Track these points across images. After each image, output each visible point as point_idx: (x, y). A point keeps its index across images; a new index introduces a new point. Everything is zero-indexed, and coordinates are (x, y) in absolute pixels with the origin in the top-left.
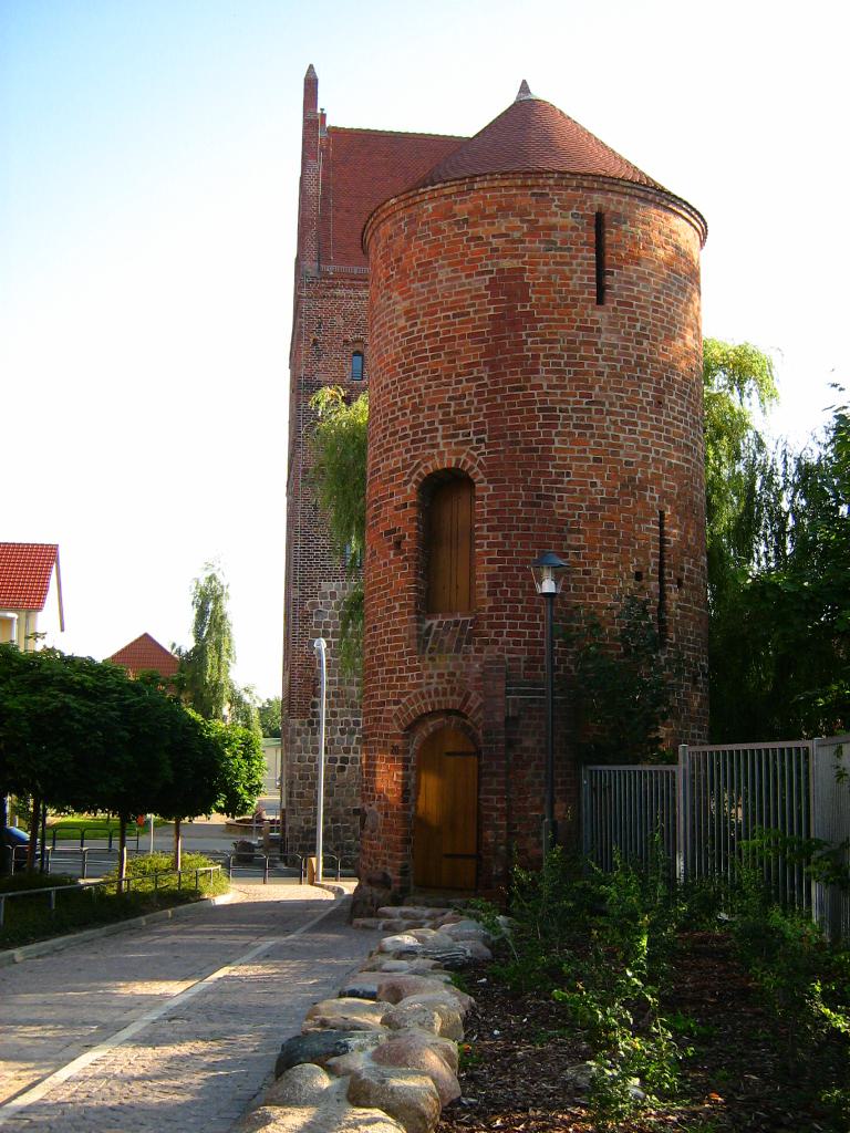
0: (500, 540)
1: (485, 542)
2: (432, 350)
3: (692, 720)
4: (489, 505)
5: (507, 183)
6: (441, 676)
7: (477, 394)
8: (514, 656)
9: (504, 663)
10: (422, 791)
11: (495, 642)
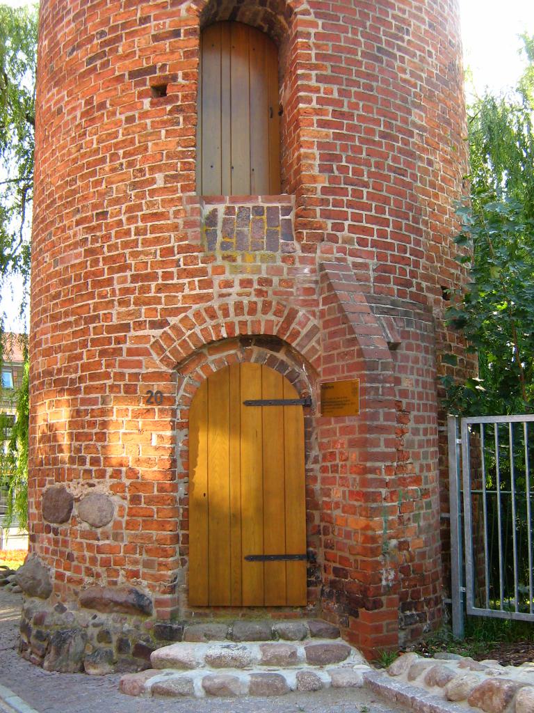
0: (336, 95)
1: (314, 96)
4: (317, 47)
6: (246, 283)
8: (360, 260)
9: (346, 268)
10: (201, 460)
11: (333, 239)
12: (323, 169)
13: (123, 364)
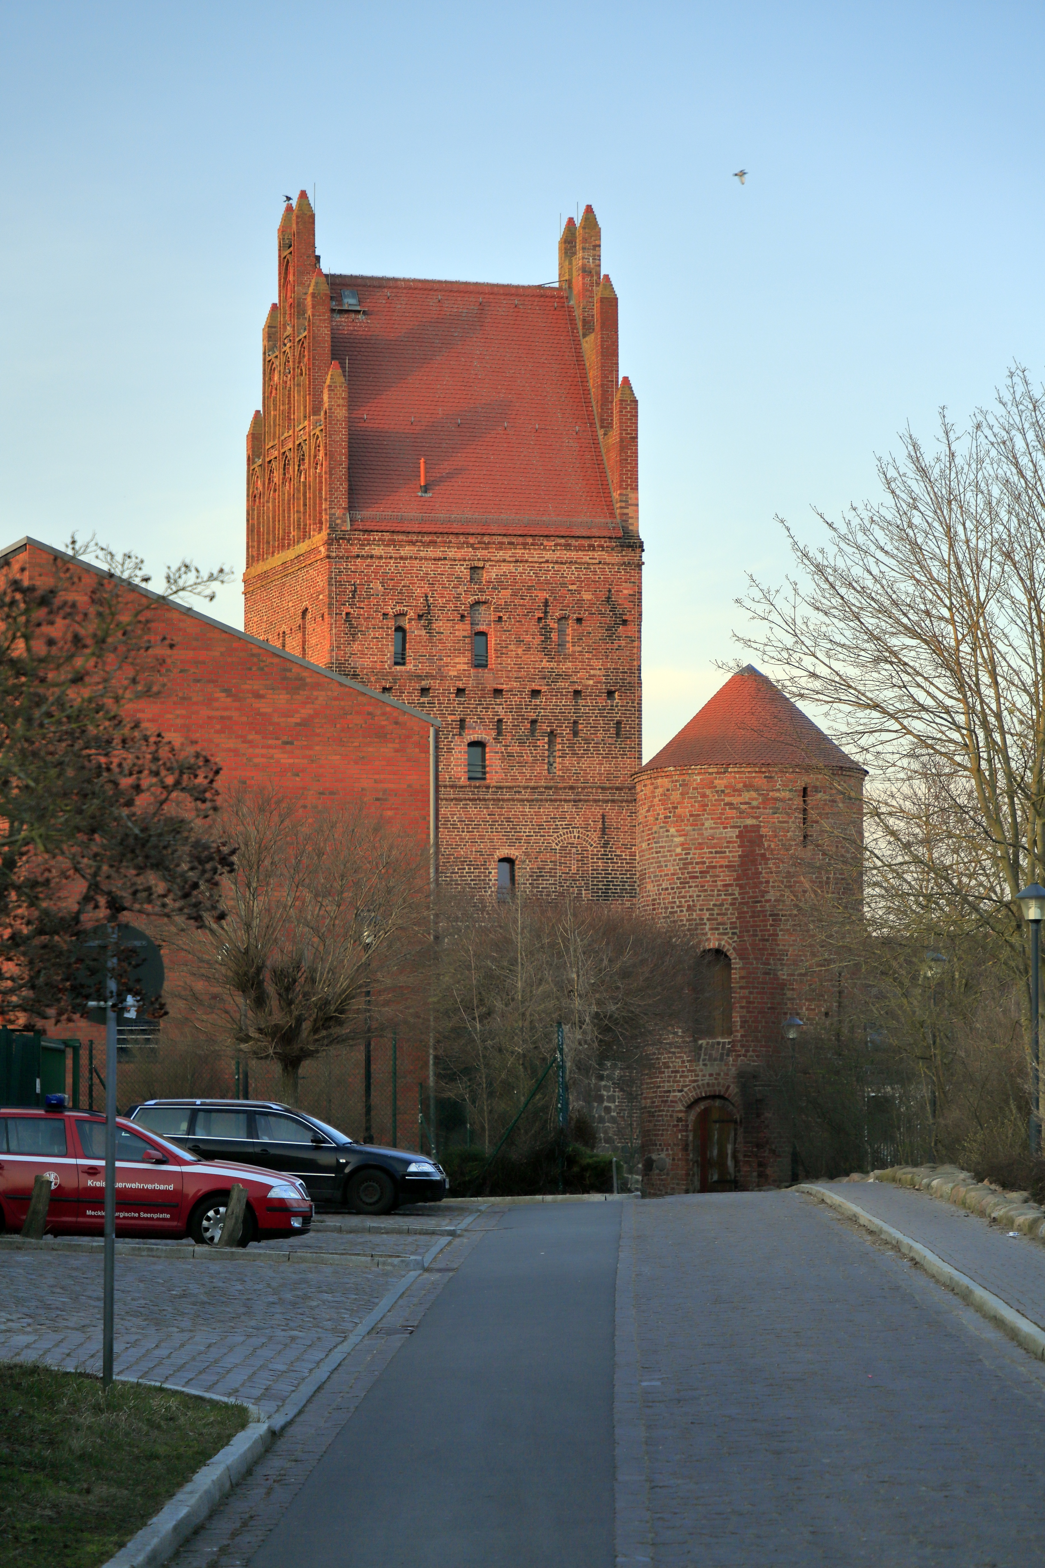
2: (701, 872)
3: (313, 988)
5: (750, 770)
6: (711, 1075)
7: (731, 904)
12: (741, 1027)
13: (669, 1106)
